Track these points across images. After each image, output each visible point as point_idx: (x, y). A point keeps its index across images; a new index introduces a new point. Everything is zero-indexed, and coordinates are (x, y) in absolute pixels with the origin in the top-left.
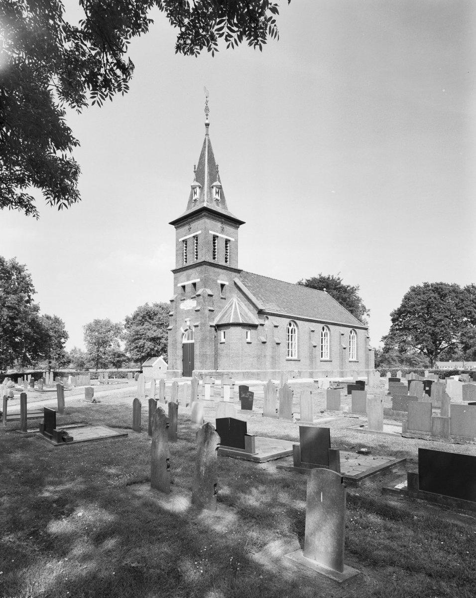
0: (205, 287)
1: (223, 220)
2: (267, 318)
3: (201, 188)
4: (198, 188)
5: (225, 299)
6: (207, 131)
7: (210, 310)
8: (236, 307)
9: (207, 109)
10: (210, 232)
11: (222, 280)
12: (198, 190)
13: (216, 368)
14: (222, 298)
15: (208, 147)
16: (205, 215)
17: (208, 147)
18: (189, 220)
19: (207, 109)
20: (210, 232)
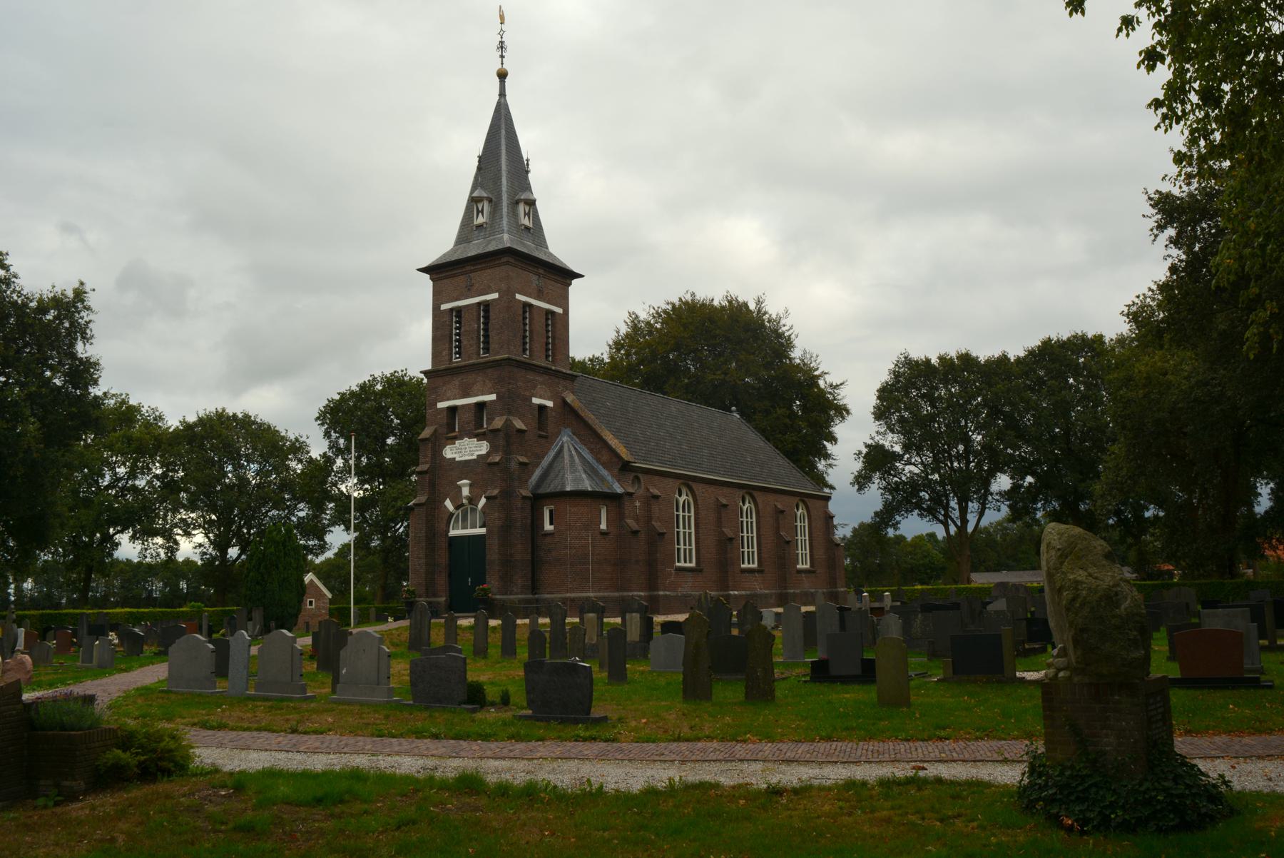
0: (510, 413)
1: (541, 271)
2: (637, 478)
3: (495, 203)
4: (486, 204)
5: (546, 437)
6: (502, 94)
7: (522, 464)
8: (571, 456)
9: (502, 46)
10: (518, 297)
11: (541, 397)
12: (486, 206)
13: (534, 588)
14: (541, 436)
15: (502, 131)
16: (507, 263)
17: (502, 131)
18: (468, 268)
19: (502, 46)
20: (518, 297)
